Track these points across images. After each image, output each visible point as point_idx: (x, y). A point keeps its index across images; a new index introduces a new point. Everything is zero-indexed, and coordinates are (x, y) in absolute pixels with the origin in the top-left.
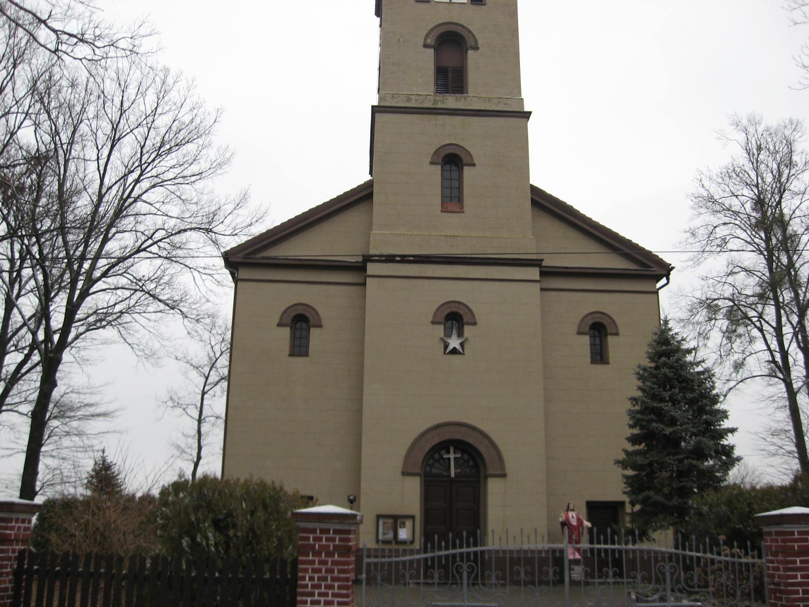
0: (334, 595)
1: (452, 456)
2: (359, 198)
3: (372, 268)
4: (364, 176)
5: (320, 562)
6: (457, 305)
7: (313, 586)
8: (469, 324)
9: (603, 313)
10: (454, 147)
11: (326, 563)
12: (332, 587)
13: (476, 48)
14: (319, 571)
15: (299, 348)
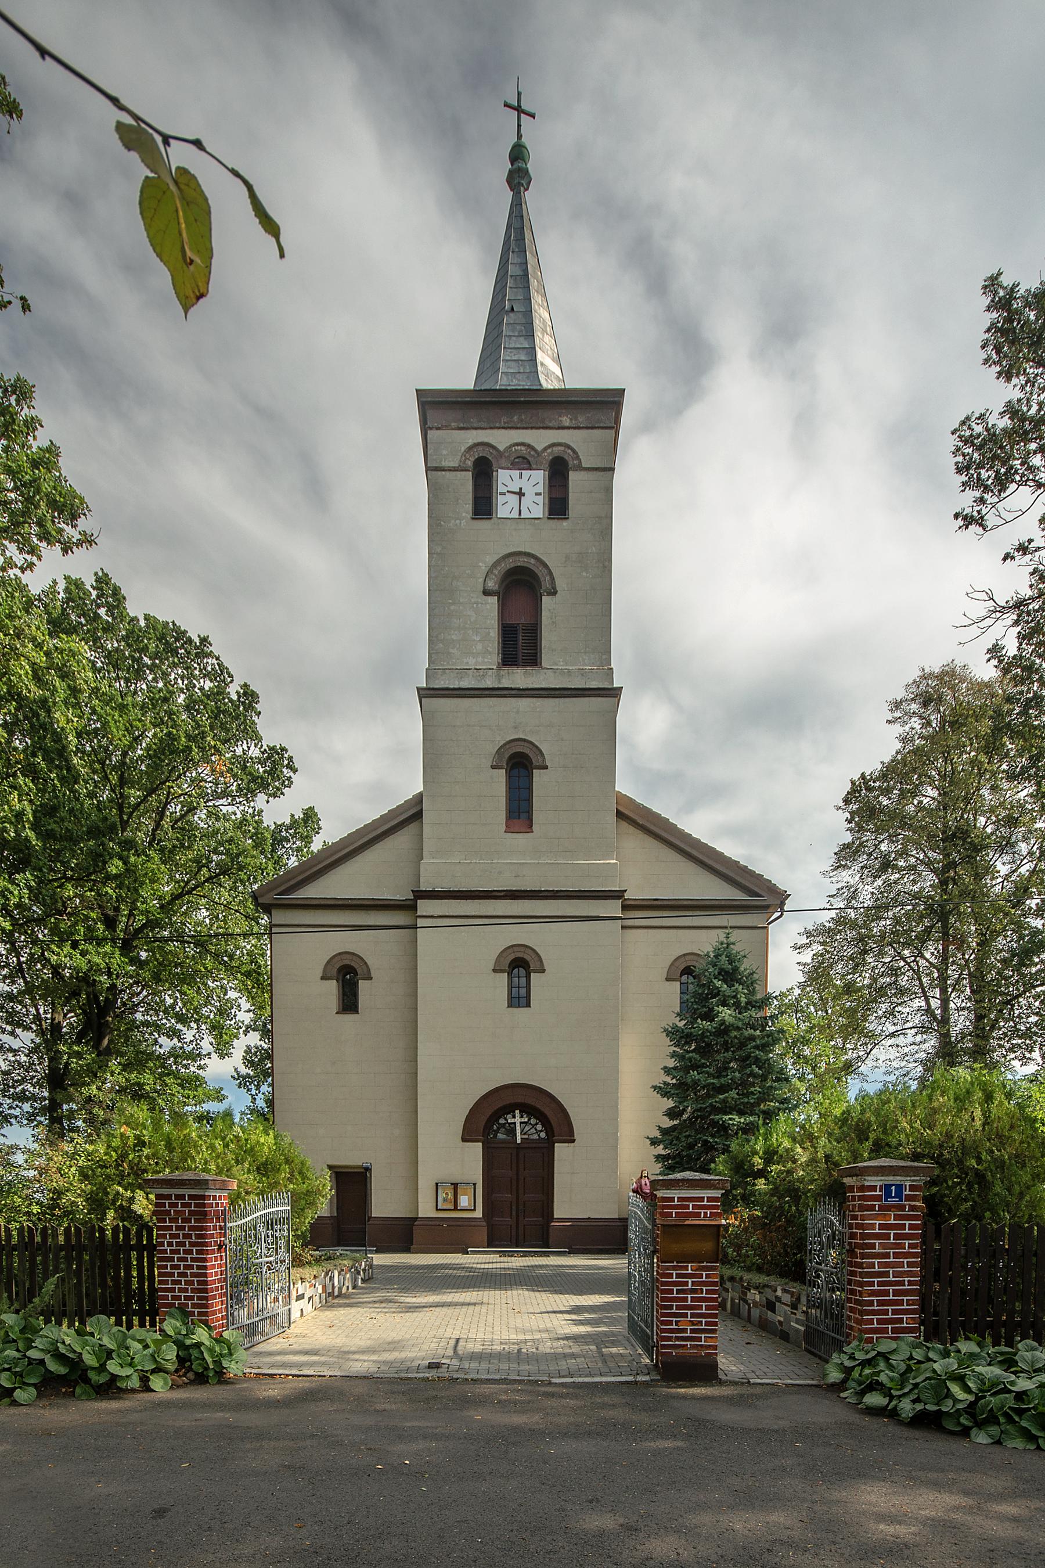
0: (193, 1260)
1: (518, 1120)
2: (412, 815)
3: (425, 907)
4: (416, 786)
5: (178, 1228)
6: (522, 949)
7: (172, 1252)
8: (535, 971)
9: (353, 954)
10: (522, 743)
11: (183, 1228)
12: (191, 1252)
13: (553, 593)
14: (177, 1236)
15: (349, 1003)
